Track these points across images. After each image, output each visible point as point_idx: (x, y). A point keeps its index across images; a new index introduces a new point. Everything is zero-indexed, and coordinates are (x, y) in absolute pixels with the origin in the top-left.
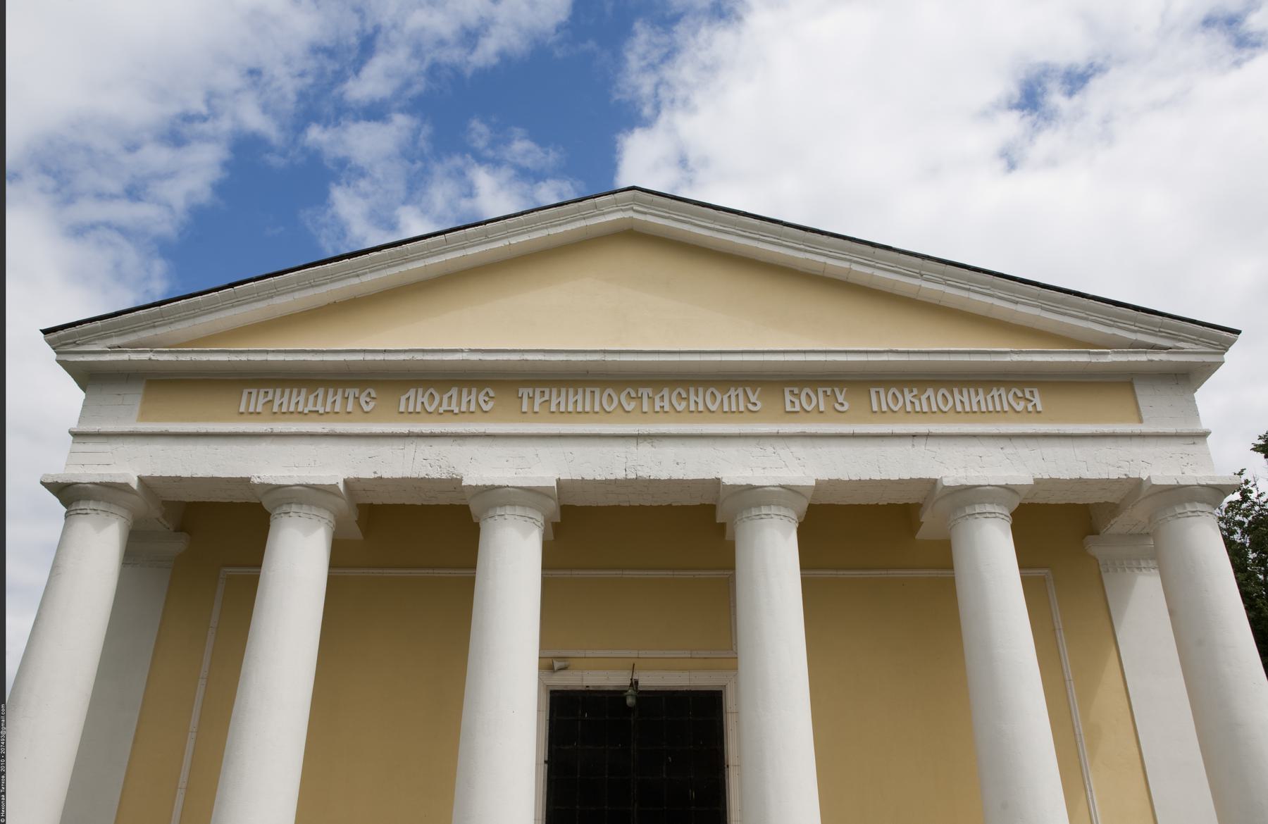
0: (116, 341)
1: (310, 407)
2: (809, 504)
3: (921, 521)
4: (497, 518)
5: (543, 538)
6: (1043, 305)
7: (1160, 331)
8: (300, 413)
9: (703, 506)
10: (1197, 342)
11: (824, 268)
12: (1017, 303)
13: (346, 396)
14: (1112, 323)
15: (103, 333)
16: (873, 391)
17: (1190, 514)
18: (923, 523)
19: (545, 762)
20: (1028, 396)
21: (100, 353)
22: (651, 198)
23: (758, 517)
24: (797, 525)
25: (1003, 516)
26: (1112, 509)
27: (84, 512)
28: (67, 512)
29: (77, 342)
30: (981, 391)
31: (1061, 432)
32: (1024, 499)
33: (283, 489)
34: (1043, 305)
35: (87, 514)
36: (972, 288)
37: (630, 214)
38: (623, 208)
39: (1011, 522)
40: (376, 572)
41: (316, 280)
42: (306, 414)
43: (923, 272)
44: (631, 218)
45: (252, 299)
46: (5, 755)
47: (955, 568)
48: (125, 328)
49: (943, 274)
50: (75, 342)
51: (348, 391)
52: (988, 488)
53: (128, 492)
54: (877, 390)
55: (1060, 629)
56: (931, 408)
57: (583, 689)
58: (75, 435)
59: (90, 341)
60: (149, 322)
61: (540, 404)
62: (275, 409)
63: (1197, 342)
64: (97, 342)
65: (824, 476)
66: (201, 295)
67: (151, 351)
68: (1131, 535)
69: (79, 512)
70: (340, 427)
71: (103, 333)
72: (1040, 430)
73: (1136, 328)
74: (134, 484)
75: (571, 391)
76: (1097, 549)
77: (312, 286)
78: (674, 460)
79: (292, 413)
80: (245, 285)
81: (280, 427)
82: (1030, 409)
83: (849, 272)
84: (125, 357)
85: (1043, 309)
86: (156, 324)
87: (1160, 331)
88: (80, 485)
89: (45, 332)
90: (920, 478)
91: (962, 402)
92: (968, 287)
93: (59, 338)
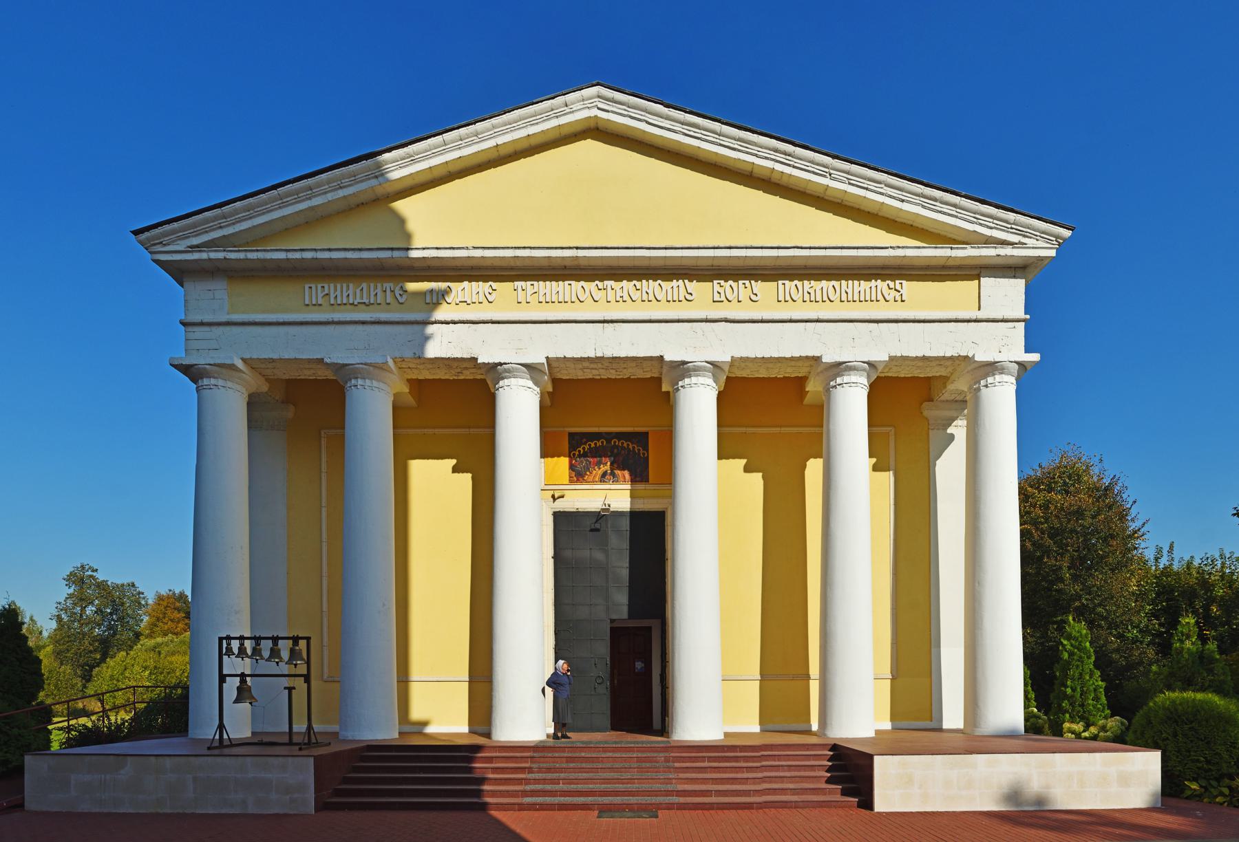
0: (196, 241)
1: (358, 300)
2: (250, 396)
3: (807, 390)
4: (505, 388)
5: (342, 437)
6: (923, 204)
7: (1012, 228)
8: (351, 304)
9: (727, 458)
10: (1038, 238)
11: (753, 168)
12: (903, 201)
13: (384, 289)
14: (975, 220)
15: (181, 234)
16: (307, 287)
17: (997, 384)
18: (808, 391)
19: (668, 688)
20: (898, 287)
21: (178, 251)
22: (458, 134)
23: (689, 386)
24: (717, 392)
25: (862, 386)
26: (944, 380)
27: (209, 387)
28: (197, 388)
29: (164, 243)
30: (351, 285)
31: (251, 320)
32: (880, 373)
33: (347, 367)
34: (923, 204)
35: (211, 389)
36: (869, 187)
37: (595, 112)
38: (589, 105)
39: (868, 390)
40: (777, 430)
41: (343, 181)
42: (356, 305)
43: (832, 171)
44: (596, 116)
45: (294, 201)
46: (1058, 731)
47: (346, 429)
48: (198, 229)
49: (848, 173)
50: (161, 243)
51: (385, 285)
52: (855, 363)
53: (237, 371)
54: (901, 281)
55: (548, 626)
56: (217, 747)
57: (575, 510)
58: (979, 310)
59: (174, 241)
60: (216, 223)
61: (323, 297)
62: (332, 302)
63: (1038, 238)
64: (178, 242)
65: (738, 354)
66: (252, 197)
67: (224, 250)
68: (956, 401)
69: (204, 387)
70: (383, 316)
71: (181, 234)
72: (564, 317)
73: (993, 225)
74: (874, 460)
75: (856, 282)
76: (929, 412)
77: (341, 188)
78: (686, 353)
79: (345, 304)
80: (286, 187)
81: (337, 316)
82: (898, 298)
83: (826, 189)
84: (204, 256)
85: (923, 207)
86: (222, 225)
87: (1012, 228)
88: (200, 366)
89: (136, 233)
90: (724, 180)
91: (847, 293)
92: (866, 186)
93: (148, 239)
